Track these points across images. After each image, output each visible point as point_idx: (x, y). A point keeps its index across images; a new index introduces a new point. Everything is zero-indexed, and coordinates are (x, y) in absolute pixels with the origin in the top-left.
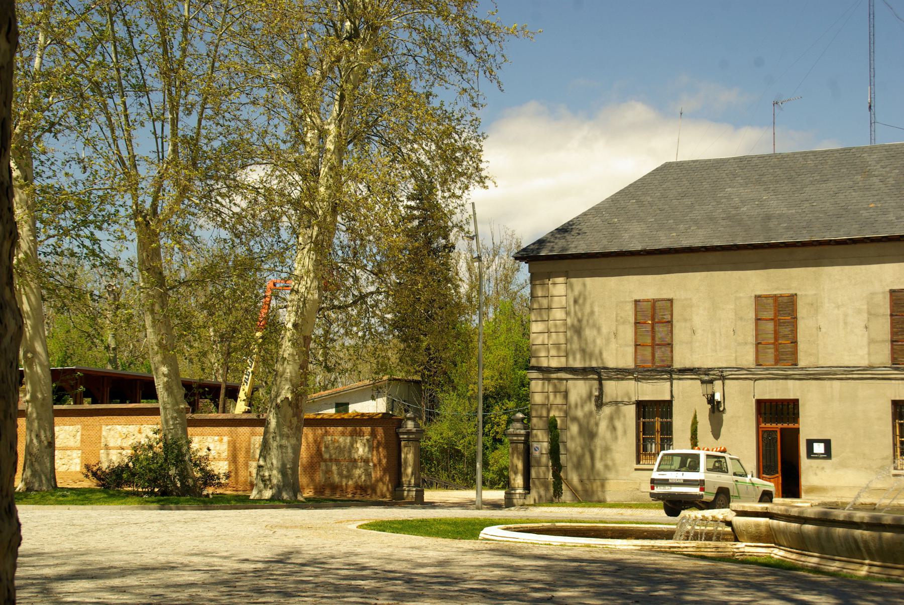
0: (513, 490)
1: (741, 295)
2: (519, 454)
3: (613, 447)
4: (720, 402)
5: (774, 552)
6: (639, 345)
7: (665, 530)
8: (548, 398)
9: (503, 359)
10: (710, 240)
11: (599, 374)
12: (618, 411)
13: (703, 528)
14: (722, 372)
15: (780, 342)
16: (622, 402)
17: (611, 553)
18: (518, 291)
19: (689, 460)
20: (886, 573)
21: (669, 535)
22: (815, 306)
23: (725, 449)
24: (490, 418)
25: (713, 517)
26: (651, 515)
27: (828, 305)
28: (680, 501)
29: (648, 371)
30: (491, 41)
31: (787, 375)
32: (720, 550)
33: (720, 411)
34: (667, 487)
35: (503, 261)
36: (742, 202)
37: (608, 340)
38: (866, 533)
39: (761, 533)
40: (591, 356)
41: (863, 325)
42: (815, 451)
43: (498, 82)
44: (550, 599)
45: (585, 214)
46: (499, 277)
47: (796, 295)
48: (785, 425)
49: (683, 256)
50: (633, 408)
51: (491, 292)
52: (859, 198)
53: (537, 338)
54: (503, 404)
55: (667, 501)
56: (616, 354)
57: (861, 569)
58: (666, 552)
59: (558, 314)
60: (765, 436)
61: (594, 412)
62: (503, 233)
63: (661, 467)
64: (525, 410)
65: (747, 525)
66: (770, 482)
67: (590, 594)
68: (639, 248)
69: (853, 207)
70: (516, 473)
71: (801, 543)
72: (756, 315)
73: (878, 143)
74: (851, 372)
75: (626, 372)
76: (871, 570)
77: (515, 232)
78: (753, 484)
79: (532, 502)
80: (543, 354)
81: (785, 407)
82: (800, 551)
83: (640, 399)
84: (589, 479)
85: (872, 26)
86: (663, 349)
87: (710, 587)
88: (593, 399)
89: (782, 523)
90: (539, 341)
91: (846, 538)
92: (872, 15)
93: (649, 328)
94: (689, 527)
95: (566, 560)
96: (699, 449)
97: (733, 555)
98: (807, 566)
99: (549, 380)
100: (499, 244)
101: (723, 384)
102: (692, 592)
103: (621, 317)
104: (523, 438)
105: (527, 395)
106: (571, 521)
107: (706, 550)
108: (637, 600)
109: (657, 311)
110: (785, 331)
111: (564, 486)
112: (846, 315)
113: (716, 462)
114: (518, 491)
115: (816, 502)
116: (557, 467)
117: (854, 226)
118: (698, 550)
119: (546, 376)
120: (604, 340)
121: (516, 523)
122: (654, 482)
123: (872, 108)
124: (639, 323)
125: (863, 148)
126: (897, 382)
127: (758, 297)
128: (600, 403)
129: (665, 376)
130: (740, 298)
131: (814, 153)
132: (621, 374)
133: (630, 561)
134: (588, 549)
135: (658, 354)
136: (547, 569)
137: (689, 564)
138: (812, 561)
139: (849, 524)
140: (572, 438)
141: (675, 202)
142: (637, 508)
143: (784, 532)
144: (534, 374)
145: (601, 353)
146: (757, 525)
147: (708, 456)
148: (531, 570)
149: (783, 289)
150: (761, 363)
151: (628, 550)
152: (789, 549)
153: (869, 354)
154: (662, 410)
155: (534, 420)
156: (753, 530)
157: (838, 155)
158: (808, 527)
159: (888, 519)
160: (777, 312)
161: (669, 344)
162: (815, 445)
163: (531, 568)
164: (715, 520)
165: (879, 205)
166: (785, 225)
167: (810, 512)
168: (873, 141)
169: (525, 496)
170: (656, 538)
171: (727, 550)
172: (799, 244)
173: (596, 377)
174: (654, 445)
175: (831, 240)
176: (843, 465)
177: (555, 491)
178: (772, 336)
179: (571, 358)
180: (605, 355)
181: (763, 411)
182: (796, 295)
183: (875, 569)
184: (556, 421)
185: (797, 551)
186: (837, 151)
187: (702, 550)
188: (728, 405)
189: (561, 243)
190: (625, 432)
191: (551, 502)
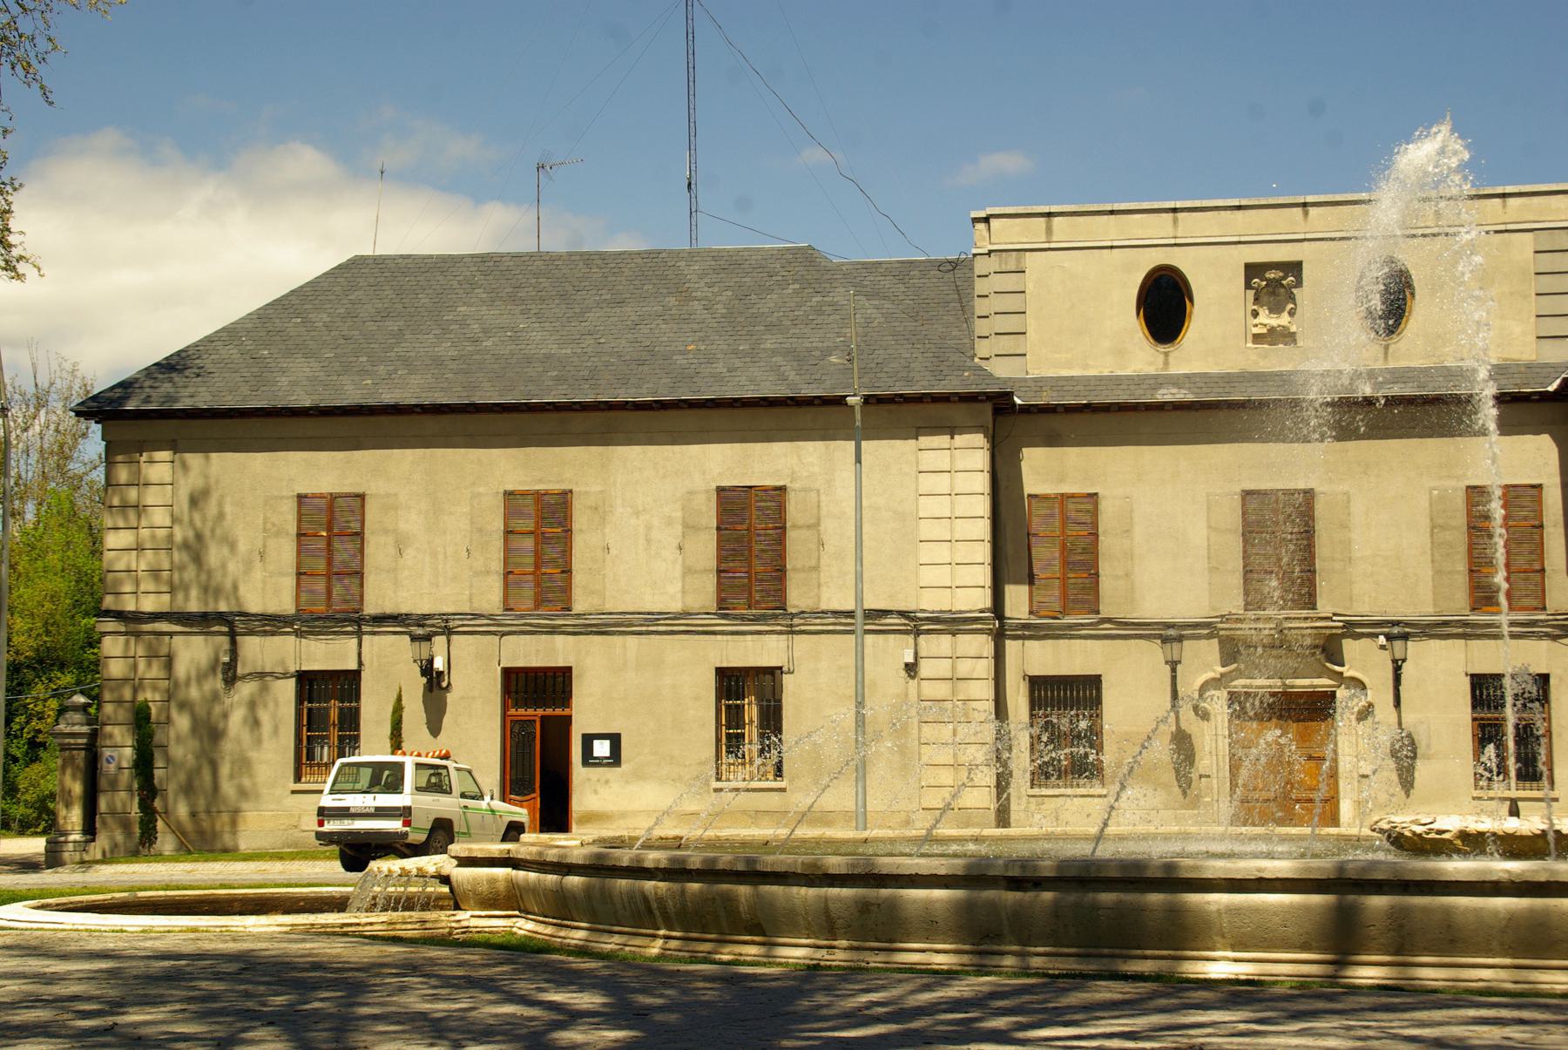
0: (62, 835)
1: (482, 490)
2: (76, 768)
3: (253, 755)
4: (442, 672)
5: (517, 925)
6: (305, 573)
7: (338, 895)
8: (135, 667)
9: (52, 597)
10: (430, 394)
11: (231, 624)
12: (264, 689)
13: (399, 889)
14: (447, 621)
15: (544, 570)
16: (271, 674)
17: (234, 940)
18: (86, 474)
19: (387, 773)
20: (690, 948)
21: (340, 904)
22: (601, 512)
23: (448, 752)
24: (25, 706)
25: (419, 869)
26: (317, 870)
27: (621, 510)
28: (369, 845)
29: (319, 618)
30: (25, 9)
31: (553, 627)
32: (428, 925)
33: (442, 688)
34: (346, 822)
35: (55, 418)
36: (485, 331)
37: (248, 566)
38: (662, 886)
39: (497, 893)
40: (218, 592)
41: (675, 543)
42: (596, 754)
43: (42, 87)
44: (109, 1030)
45: (209, 340)
46: (46, 446)
47: (571, 491)
48: (549, 711)
49: (384, 420)
50: (291, 684)
51: (30, 474)
52: (671, 335)
53: (118, 559)
54: (50, 680)
55: (346, 845)
56: (263, 589)
57: (653, 944)
58: (334, 934)
59: (160, 517)
60: (516, 729)
61: (221, 692)
62: (54, 366)
63: (338, 787)
64: (92, 689)
65: (476, 882)
66: (521, 806)
67: (187, 1015)
68: (307, 404)
69: (662, 349)
70: (68, 805)
71: (560, 907)
72: (506, 525)
73: (703, 244)
74: (655, 622)
75: (280, 621)
76: (667, 946)
77: (79, 367)
78: (492, 811)
79: (99, 856)
80: (128, 588)
81: (550, 682)
82: (559, 921)
83: (304, 668)
84: (208, 812)
85: (691, 53)
86: (346, 581)
87: (402, 989)
88: (219, 669)
89: (532, 876)
90: (121, 566)
91: (631, 895)
92: (690, 35)
93: (322, 545)
94: (377, 889)
95: (149, 957)
96: (404, 754)
97: (450, 934)
98: (569, 945)
99: (138, 635)
100: (46, 385)
101: (449, 641)
102: (370, 1001)
103: (274, 525)
104: (84, 741)
105: (97, 663)
106: (167, 888)
107: (404, 927)
108: (271, 1019)
109: (337, 515)
110: (551, 552)
111: (160, 824)
112: (649, 528)
113: (431, 775)
114: (71, 838)
115: (589, 838)
116: (148, 790)
117: (663, 381)
118: (391, 927)
119: (132, 627)
120: (240, 565)
121: (62, 895)
122: (324, 814)
123: (693, 186)
124: (304, 535)
125: (679, 252)
126: (725, 637)
127: (509, 495)
128: (231, 675)
129: (349, 629)
130: (480, 494)
131: (602, 256)
132: (272, 624)
133: (267, 953)
134: (192, 936)
135: (337, 590)
136: (112, 973)
137: (371, 952)
138: (577, 935)
139: (638, 871)
140: (179, 739)
141: (371, 326)
142: (293, 859)
143: (533, 890)
144: (110, 625)
145: (235, 587)
146: (492, 881)
147: (419, 766)
148: (80, 979)
149: (550, 481)
150: (511, 606)
151: (266, 933)
152: (541, 919)
153: (684, 592)
154: (343, 688)
155: (108, 709)
156: (484, 888)
157: (640, 261)
158: (574, 881)
159: (695, 860)
160: (541, 519)
161: (357, 573)
162: (596, 743)
163: (81, 975)
164: (421, 874)
165: (703, 348)
166: (555, 373)
167: (578, 855)
168: (694, 241)
169: (83, 846)
170: (321, 911)
171: (439, 926)
172: (577, 407)
173: (226, 629)
174: (326, 749)
175: (627, 402)
176: (639, 776)
177: (142, 835)
178: (530, 560)
179: (180, 596)
180: (242, 590)
181: (513, 688)
182: (571, 491)
183: (673, 944)
184: (149, 708)
185: (555, 921)
186: (639, 253)
187: (398, 926)
188: (456, 678)
189: (166, 388)
190: (276, 730)
191: (134, 854)
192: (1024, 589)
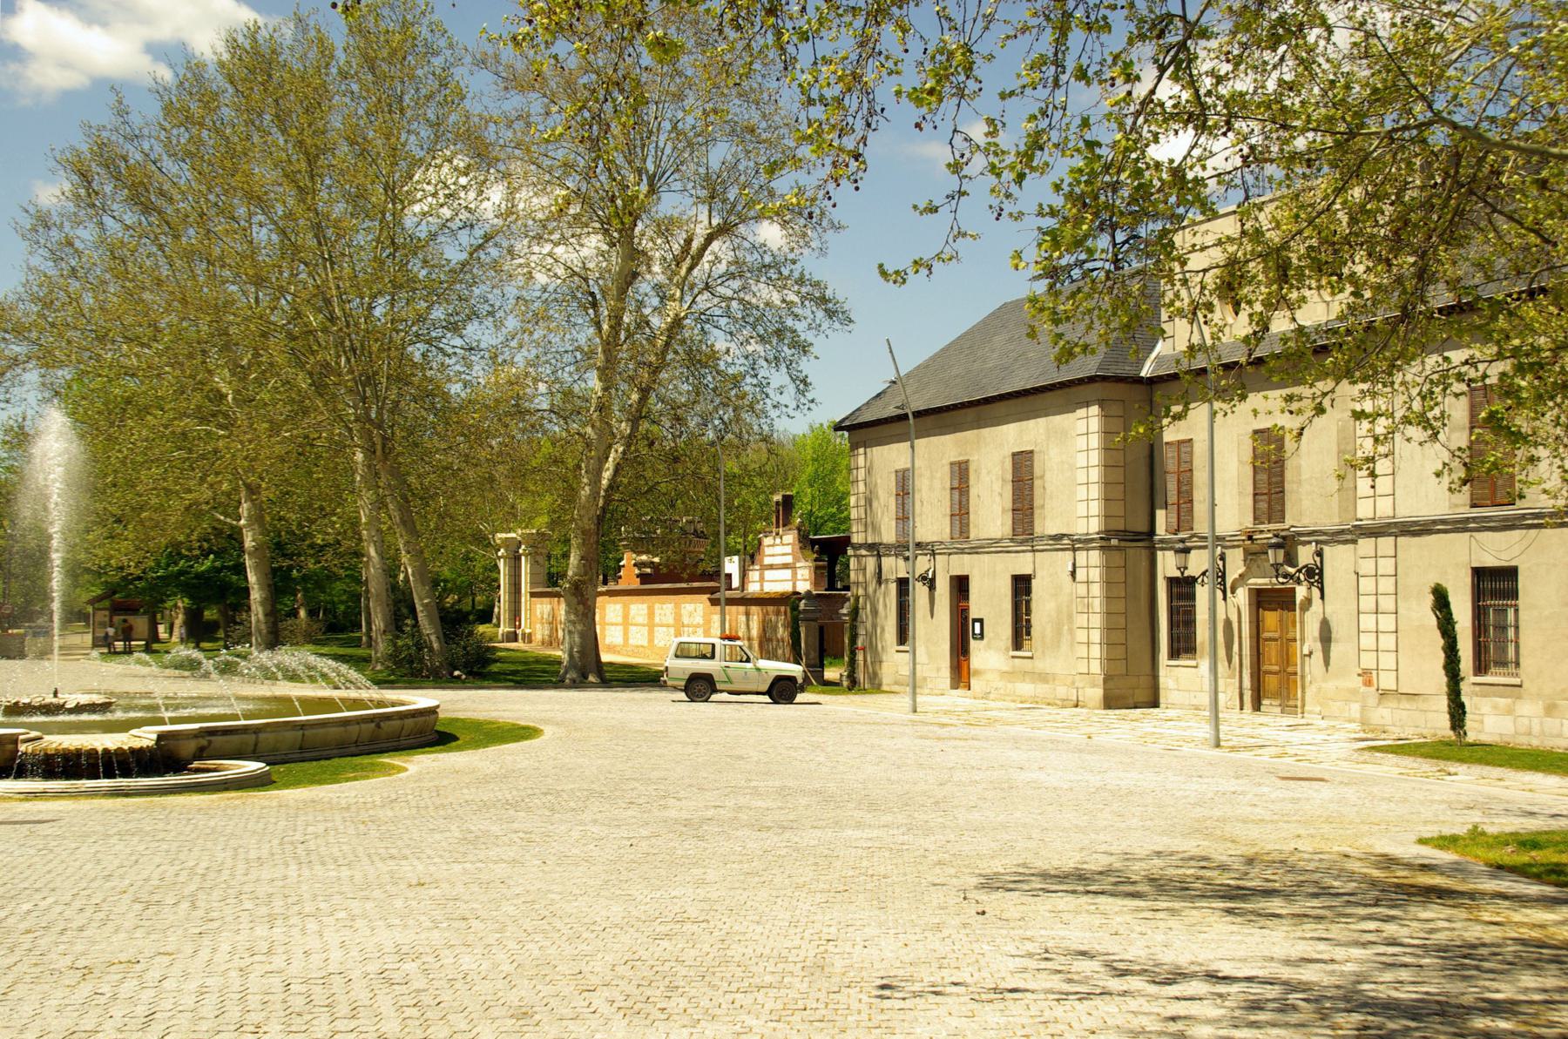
192: (1164, 512)
